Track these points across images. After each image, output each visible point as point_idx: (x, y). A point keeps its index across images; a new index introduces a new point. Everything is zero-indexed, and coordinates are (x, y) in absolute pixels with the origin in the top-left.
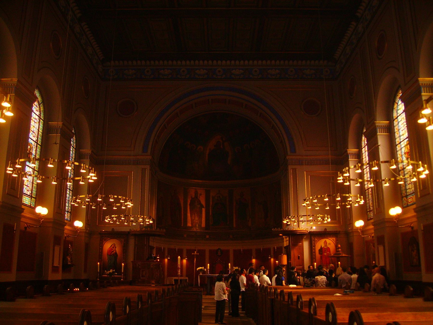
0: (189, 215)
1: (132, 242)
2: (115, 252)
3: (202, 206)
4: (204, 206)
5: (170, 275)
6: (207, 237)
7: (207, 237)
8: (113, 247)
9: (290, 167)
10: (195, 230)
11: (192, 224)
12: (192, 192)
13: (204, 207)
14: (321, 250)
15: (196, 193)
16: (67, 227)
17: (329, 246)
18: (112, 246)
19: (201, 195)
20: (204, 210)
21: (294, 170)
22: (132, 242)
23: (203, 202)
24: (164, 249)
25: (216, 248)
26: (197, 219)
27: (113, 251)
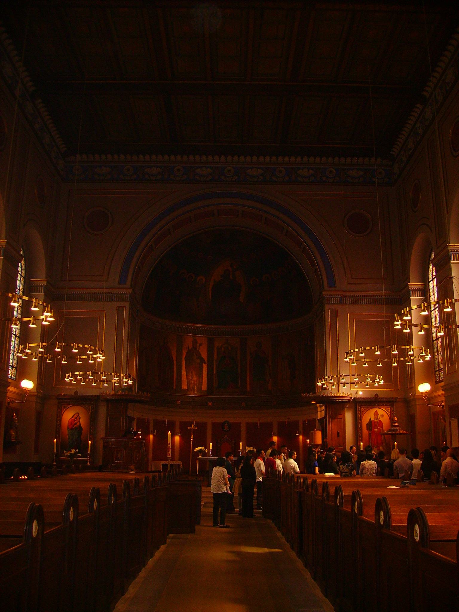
0: (184, 373)
1: (103, 410)
2: (78, 424)
3: (203, 361)
4: (206, 360)
5: (156, 457)
6: (210, 404)
7: (210, 404)
8: (76, 418)
9: (327, 307)
10: (192, 394)
11: (188, 386)
12: (189, 342)
13: (205, 363)
14: (370, 425)
15: (195, 342)
16: (11, 389)
17: (381, 419)
18: (75, 416)
19: (201, 345)
20: (205, 366)
21: (334, 311)
22: (103, 410)
23: (204, 356)
24: (148, 420)
25: (221, 420)
26: (195, 378)
27: (76, 424)
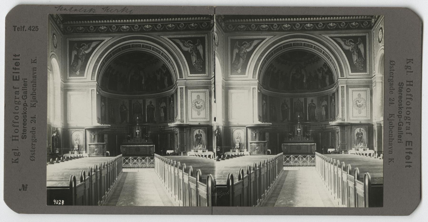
17: (362, 132)
